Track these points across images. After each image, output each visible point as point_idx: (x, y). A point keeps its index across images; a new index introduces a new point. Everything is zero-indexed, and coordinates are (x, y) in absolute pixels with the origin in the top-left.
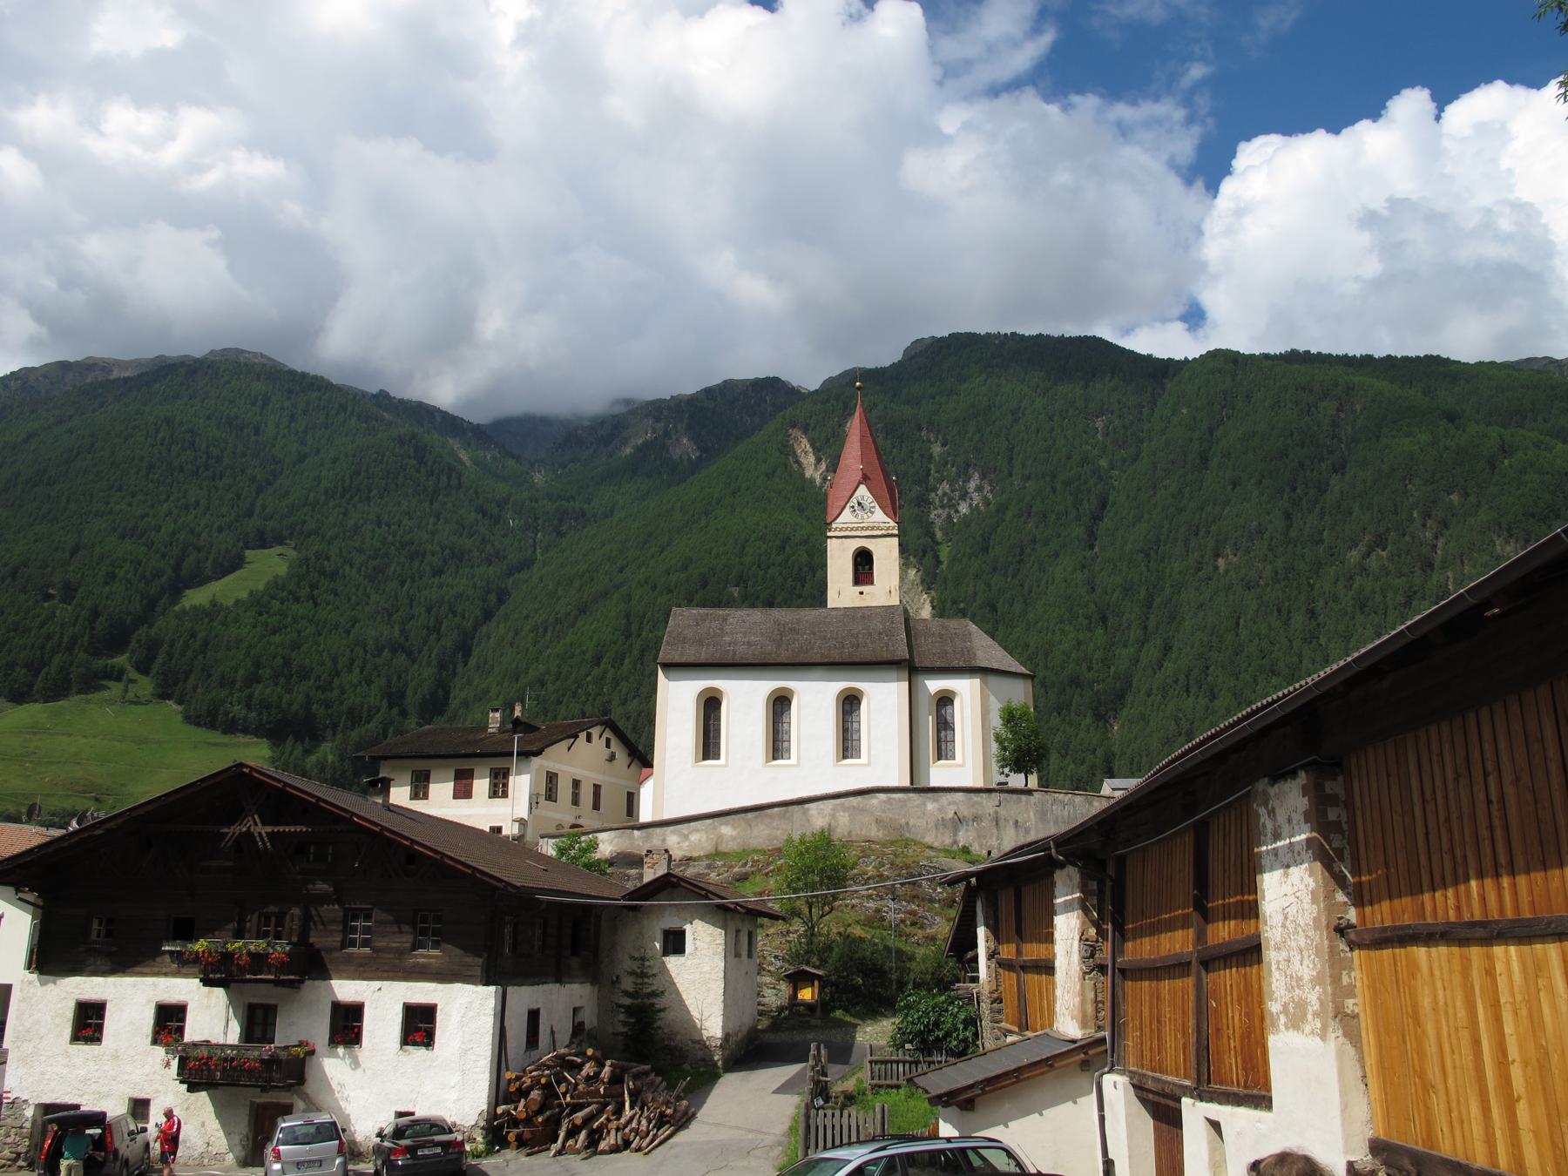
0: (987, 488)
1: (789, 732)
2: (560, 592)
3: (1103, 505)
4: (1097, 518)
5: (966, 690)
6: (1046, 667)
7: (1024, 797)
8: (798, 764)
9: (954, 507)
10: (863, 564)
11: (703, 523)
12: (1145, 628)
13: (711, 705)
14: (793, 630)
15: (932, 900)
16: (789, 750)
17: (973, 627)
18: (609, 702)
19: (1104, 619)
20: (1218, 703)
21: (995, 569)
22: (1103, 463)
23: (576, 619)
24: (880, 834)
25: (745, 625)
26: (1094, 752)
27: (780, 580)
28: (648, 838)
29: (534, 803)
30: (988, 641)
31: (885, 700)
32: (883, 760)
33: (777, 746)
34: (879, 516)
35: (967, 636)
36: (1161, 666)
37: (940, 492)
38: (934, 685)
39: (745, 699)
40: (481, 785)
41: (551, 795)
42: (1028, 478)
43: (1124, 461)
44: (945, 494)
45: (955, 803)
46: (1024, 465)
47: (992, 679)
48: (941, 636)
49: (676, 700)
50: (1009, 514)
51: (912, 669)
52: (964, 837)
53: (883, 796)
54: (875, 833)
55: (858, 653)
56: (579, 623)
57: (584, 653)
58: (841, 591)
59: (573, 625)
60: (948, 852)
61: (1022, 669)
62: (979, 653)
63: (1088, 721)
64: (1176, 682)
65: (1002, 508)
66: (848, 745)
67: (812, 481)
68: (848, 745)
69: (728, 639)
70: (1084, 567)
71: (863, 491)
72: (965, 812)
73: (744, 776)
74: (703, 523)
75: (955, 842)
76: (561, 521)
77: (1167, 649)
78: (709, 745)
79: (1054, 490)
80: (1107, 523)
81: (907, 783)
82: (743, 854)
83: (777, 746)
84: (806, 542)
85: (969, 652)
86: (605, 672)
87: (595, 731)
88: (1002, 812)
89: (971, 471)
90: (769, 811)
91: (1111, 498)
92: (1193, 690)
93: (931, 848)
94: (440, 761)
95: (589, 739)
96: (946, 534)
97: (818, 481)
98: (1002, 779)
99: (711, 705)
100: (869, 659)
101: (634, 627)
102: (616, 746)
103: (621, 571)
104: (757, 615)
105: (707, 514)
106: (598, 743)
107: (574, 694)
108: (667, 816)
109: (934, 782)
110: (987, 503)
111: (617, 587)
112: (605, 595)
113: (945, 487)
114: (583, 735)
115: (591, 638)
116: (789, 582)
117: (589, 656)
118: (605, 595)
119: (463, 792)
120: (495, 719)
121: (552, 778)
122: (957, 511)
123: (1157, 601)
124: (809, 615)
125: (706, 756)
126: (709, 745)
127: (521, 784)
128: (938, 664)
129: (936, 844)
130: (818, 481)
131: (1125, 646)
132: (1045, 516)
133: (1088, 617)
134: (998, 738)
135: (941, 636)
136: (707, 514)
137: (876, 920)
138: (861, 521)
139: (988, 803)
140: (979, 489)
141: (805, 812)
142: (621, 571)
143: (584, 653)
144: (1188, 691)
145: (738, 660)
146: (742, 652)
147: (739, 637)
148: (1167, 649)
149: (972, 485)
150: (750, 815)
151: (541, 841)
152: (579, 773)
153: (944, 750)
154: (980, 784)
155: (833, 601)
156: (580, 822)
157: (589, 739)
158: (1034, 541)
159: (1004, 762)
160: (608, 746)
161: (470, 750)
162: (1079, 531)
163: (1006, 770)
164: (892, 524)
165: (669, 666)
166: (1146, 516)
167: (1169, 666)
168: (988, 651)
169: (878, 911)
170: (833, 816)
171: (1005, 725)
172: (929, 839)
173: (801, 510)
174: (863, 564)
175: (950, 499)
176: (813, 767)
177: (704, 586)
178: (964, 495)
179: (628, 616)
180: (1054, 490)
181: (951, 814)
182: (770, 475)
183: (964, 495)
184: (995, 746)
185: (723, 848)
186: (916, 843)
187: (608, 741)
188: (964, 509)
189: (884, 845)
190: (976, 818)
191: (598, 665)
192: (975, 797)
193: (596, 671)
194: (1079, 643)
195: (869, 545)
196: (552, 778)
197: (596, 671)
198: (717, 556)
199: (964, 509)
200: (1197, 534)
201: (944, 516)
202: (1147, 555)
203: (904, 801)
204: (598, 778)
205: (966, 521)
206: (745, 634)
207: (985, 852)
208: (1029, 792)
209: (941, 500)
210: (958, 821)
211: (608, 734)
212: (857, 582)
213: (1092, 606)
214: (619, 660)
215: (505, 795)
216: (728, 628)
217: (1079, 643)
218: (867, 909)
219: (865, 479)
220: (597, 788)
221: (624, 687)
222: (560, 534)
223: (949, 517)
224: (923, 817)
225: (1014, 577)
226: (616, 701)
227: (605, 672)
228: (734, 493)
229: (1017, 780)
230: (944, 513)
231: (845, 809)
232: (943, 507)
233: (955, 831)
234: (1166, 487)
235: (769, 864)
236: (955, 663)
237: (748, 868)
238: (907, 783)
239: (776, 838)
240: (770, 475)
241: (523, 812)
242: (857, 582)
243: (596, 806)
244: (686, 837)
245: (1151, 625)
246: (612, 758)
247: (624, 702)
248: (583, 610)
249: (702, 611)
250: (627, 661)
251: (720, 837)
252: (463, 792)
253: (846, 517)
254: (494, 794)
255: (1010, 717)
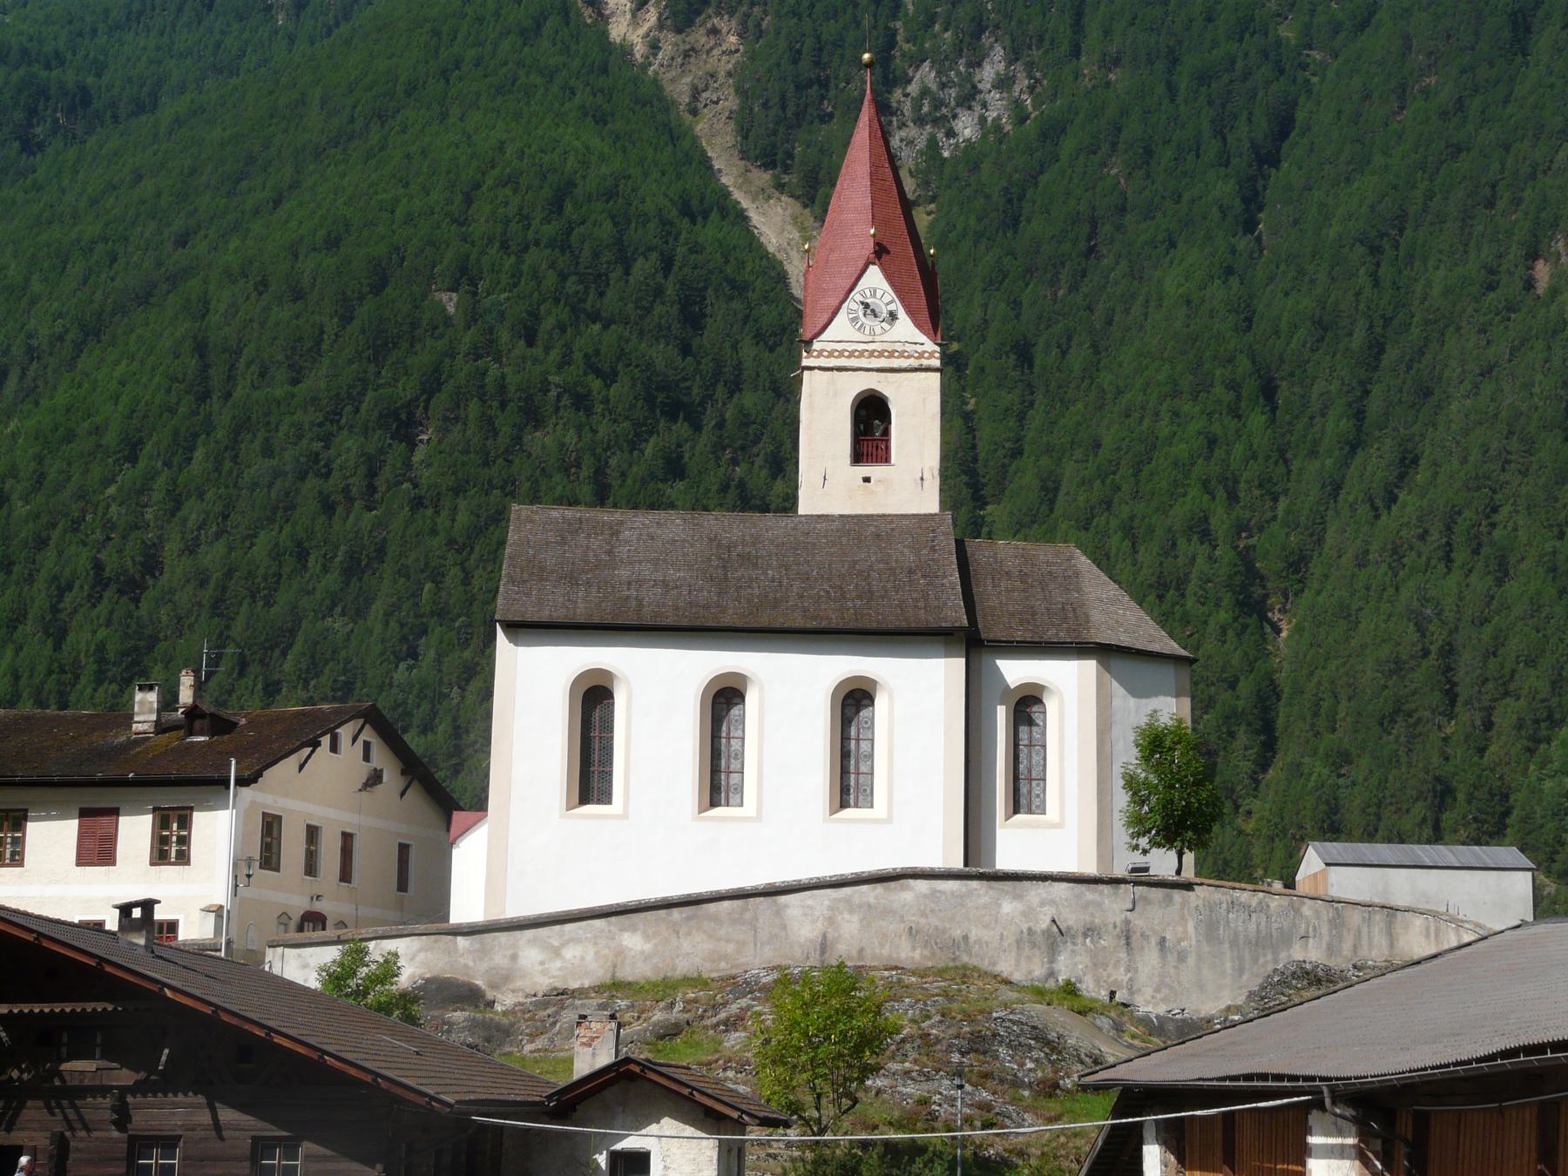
0: (1023, 82)
1: (740, 756)
2: (36, 286)
3: (1283, 126)
4: (1267, 158)
5: (1068, 685)
6: (1136, 495)
7: (1177, 895)
8: (759, 818)
9: (944, 123)
10: (871, 423)
11: (375, 137)
12: (1360, 415)
13: (594, 699)
14: (745, 558)
15: (1017, 1083)
16: (740, 789)
17: (1083, 562)
18: (158, 545)
19: (1268, 392)
20: (1512, 588)
21: (1030, 271)
22: (1288, 32)
23: (79, 348)
24: (917, 955)
25: (657, 542)
26: (1233, 685)
27: (551, 279)
28: (484, 952)
29: (241, 874)
30: (1112, 590)
31: (920, 695)
32: (913, 813)
33: (718, 781)
34: (906, 331)
35: (1072, 580)
36: (1393, 499)
37: (913, 88)
38: (1016, 671)
39: (660, 687)
40: (135, 831)
41: (270, 857)
42: (1117, 62)
43: (1337, 28)
44: (925, 92)
45: (1053, 902)
46: (1107, 33)
47: (1117, 663)
48: (1023, 577)
49: (531, 685)
50: (1068, 145)
51: (973, 643)
52: (1068, 965)
53: (922, 886)
54: (909, 954)
55: (853, 602)
56: (84, 363)
57: (98, 430)
58: (827, 480)
59: (71, 365)
60: (1039, 993)
61: (1173, 647)
62: (1096, 616)
63: (1223, 616)
64: (1423, 537)
65: (1052, 131)
66: (849, 782)
67: (625, 50)
68: (849, 782)
69: (623, 573)
70: (1229, 271)
71: (874, 277)
72: (1070, 919)
73: (655, 839)
74: (375, 137)
75: (1052, 974)
76: (32, 112)
77: (1407, 462)
78: (591, 778)
79: (1172, 90)
80: (1288, 173)
81: (957, 863)
82: (664, 989)
83: (718, 781)
84: (610, 195)
85: (1074, 613)
86: (151, 476)
87: (345, 732)
88: (1138, 921)
89: (987, 39)
90: (712, 907)
91: (1300, 116)
92: (1460, 556)
93: (1008, 982)
94: (49, 793)
95: (334, 748)
96: (925, 184)
97: (639, 50)
98: (1138, 859)
99: (594, 699)
100: (893, 623)
101: (217, 375)
102: (381, 757)
103: (182, 241)
104: (673, 526)
105: (382, 117)
106: (350, 752)
107: (76, 526)
108: (512, 912)
109: (1005, 860)
110: (1021, 118)
111: (174, 280)
112: (144, 297)
113: (926, 75)
114: (326, 740)
115: (116, 398)
116: (571, 285)
117: (111, 438)
118: (144, 297)
119: (97, 850)
120: (145, 703)
121: (271, 825)
122: (951, 134)
123: (1391, 355)
124: (771, 526)
125: (584, 799)
126: (591, 778)
127: (216, 831)
128: (1019, 635)
129: (1017, 977)
130: (639, 50)
131: (1313, 453)
132: (1148, 152)
133: (1233, 386)
134: (1131, 783)
135: (1023, 577)
136: (382, 117)
137: (920, 1112)
138: (868, 347)
139: (1113, 905)
140: (1003, 83)
141: (779, 912)
142: (182, 241)
143: (98, 430)
144: (1448, 560)
145: (648, 620)
146: (652, 601)
147: (646, 570)
148: (1407, 462)
149: (988, 74)
150: (676, 914)
151: (271, 955)
152: (318, 812)
153: (1025, 795)
154: (1091, 869)
155: (810, 501)
156: (318, 907)
157: (334, 748)
158: (1122, 209)
159: (1138, 825)
160: (367, 758)
161: (112, 772)
162: (1224, 189)
163: (1144, 842)
164: (930, 346)
165: (523, 629)
166: (1378, 160)
167: (1408, 500)
168: (1117, 613)
169: (924, 1102)
170: (831, 921)
171: (1146, 759)
172: (1005, 967)
173: (601, 120)
174: (871, 423)
175: (938, 104)
176: (783, 829)
177: (378, 288)
178: (970, 96)
179: (201, 348)
180: (1172, 90)
181: (1044, 923)
182: (530, 32)
183: (970, 96)
184: (1122, 799)
185: (627, 973)
186: (983, 974)
187: (367, 745)
188: (966, 127)
189: (923, 973)
190: (1090, 931)
191: (133, 459)
192: (1089, 893)
193: (129, 475)
194: (1212, 442)
195: (887, 386)
196: (271, 825)
197: (129, 475)
198: (409, 219)
199: (966, 127)
200: (1490, 204)
201: (921, 143)
202: (1376, 250)
203: (960, 898)
204: (347, 819)
205: (972, 157)
206: (656, 562)
207: (1103, 995)
208: (1188, 886)
209: (917, 106)
210: (1057, 936)
211: (368, 735)
212: (858, 457)
213: (1244, 363)
214: (184, 446)
215: (183, 858)
216: (622, 551)
217: (1212, 442)
218: (904, 1097)
219: (880, 253)
220: (347, 838)
221: (192, 511)
222: (29, 146)
223: (933, 144)
224: (996, 932)
225: (1074, 288)
226: (172, 547)
227: (151, 476)
228: (445, 74)
229: (1163, 862)
230: (920, 136)
231: (851, 907)
232: (920, 121)
233: (1052, 951)
234: (1426, 93)
235: (715, 1008)
236: (1050, 635)
237: (676, 1014)
238: (957, 863)
239: (725, 957)
240: (530, 32)
241: (220, 894)
242: (858, 457)
243: (346, 876)
244: (557, 952)
245: (1374, 406)
246: (375, 778)
247: (191, 549)
248: (93, 330)
249: (570, 513)
250: (199, 454)
251: (620, 952)
252: (97, 850)
253: (841, 329)
254: (160, 856)
255: (1154, 743)
